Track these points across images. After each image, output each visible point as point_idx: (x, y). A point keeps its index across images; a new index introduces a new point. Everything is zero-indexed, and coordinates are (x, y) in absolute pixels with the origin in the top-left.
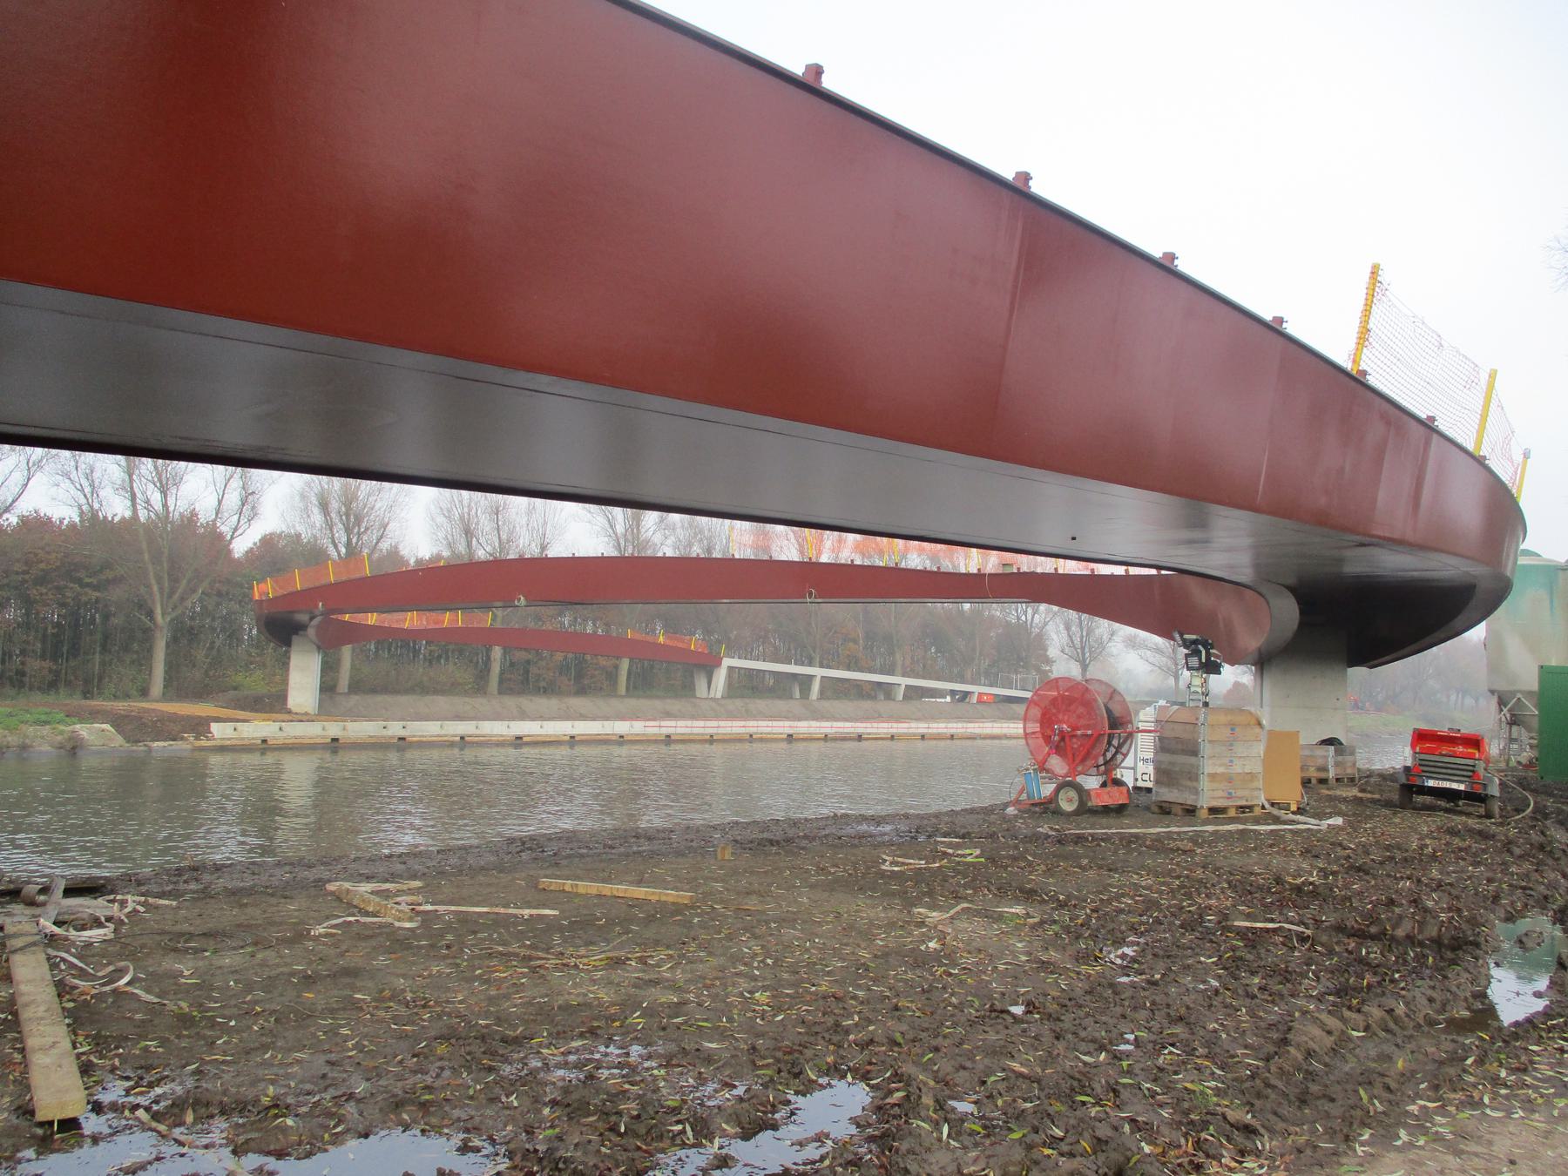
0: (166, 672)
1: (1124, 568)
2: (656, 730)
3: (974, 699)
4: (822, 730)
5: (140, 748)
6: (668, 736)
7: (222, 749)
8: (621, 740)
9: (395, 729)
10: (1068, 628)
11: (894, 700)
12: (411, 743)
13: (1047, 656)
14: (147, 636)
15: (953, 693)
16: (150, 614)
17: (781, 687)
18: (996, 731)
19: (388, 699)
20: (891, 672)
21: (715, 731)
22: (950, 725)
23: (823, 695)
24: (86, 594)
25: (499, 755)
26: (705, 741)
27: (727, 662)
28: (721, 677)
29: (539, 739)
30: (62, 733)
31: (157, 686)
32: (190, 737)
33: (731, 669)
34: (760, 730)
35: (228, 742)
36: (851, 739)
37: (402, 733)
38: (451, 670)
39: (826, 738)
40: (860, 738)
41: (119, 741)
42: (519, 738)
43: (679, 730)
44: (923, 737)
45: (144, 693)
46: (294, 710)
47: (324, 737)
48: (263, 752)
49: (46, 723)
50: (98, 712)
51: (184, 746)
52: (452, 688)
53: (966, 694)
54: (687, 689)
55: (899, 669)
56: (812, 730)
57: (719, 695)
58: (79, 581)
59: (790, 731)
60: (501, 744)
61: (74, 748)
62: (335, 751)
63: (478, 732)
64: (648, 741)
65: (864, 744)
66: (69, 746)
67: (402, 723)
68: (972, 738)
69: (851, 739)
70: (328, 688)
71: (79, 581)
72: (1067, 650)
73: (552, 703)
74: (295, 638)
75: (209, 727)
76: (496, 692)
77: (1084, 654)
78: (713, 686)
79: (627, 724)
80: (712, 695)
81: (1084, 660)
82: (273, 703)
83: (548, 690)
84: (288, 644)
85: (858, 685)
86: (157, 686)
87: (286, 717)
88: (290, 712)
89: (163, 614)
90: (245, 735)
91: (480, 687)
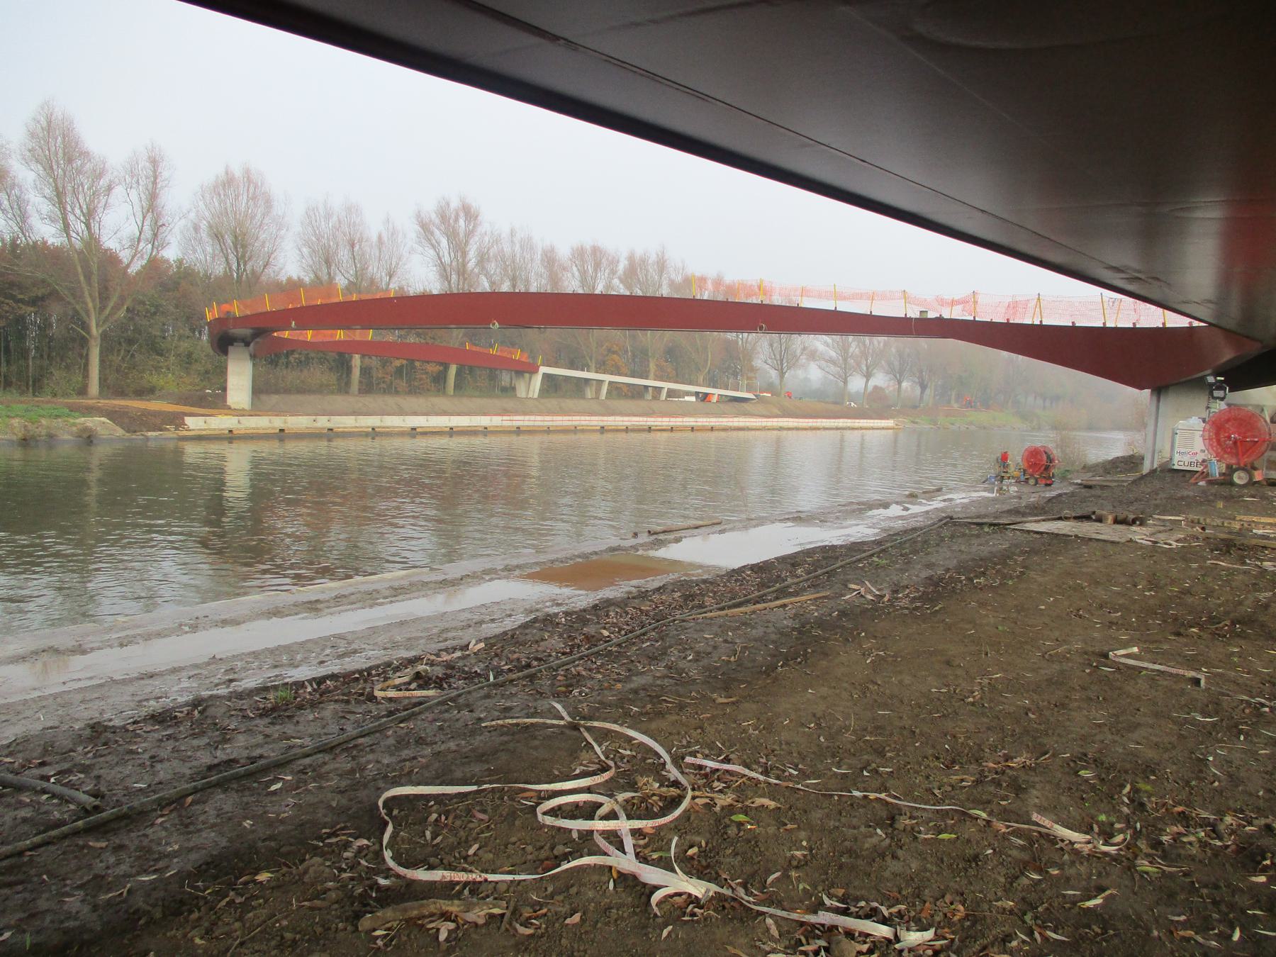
0: (100, 371)
1: (1189, 320)
2: (509, 423)
3: (715, 399)
4: (546, 424)
5: (137, 436)
6: (518, 428)
7: (200, 438)
8: (486, 431)
9: (323, 422)
10: (771, 345)
11: (1158, 401)
12: (337, 433)
13: (752, 366)
14: (84, 342)
15: (697, 394)
16: (85, 326)
17: (638, 393)
18: (741, 424)
19: (300, 397)
20: (644, 376)
21: (550, 423)
22: (685, 419)
23: (609, 392)
24: (20, 308)
25: (353, 445)
26: (367, 435)
27: (544, 370)
28: (537, 381)
29: (428, 430)
30: (74, 425)
31: (94, 387)
32: (172, 427)
33: (546, 376)
34: (584, 423)
35: (204, 433)
36: (643, 430)
37: (330, 425)
38: (318, 374)
39: (627, 430)
40: (650, 429)
41: (120, 432)
42: (414, 429)
43: (527, 423)
44: (692, 429)
45: (83, 391)
46: (233, 406)
47: (273, 428)
48: (414, 436)
49: (57, 417)
50: (92, 408)
51: (171, 432)
52: (320, 390)
53: (706, 395)
54: (509, 391)
55: (652, 375)
56: (616, 423)
57: (536, 396)
58: (13, 297)
59: (602, 424)
60: (402, 434)
61: (89, 437)
62: (282, 440)
63: (382, 425)
64: (500, 432)
65: (652, 434)
66: (85, 436)
67: (327, 418)
68: (725, 429)
69: (643, 430)
70: (259, 390)
71: (13, 297)
72: (769, 361)
73: (391, 401)
74: (230, 348)
75: (183, 420)
76: (357, 393)
77: (782, 364)
78: (531, 388)
79: (488, 418)
80: (530, 396)
81: (782, 369)
82: (215, 400)
83: (390, 390)
84: (226, 353)
85: (617, 388)
86: (94, 387)
87: (226, 411)
88: (229, 408)
89: (97, 325)
90: (213, 426)
91: (344, 388)
